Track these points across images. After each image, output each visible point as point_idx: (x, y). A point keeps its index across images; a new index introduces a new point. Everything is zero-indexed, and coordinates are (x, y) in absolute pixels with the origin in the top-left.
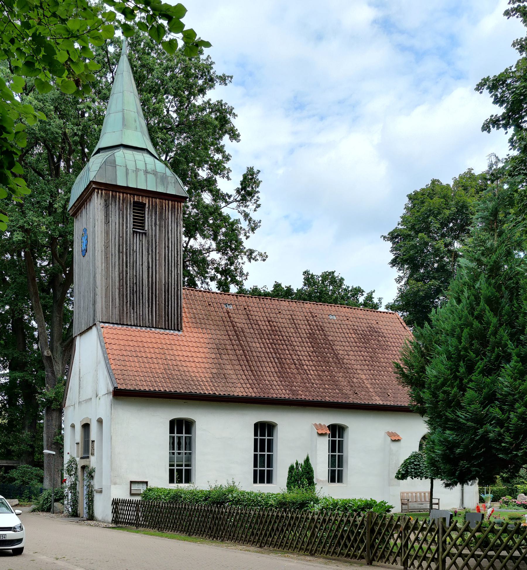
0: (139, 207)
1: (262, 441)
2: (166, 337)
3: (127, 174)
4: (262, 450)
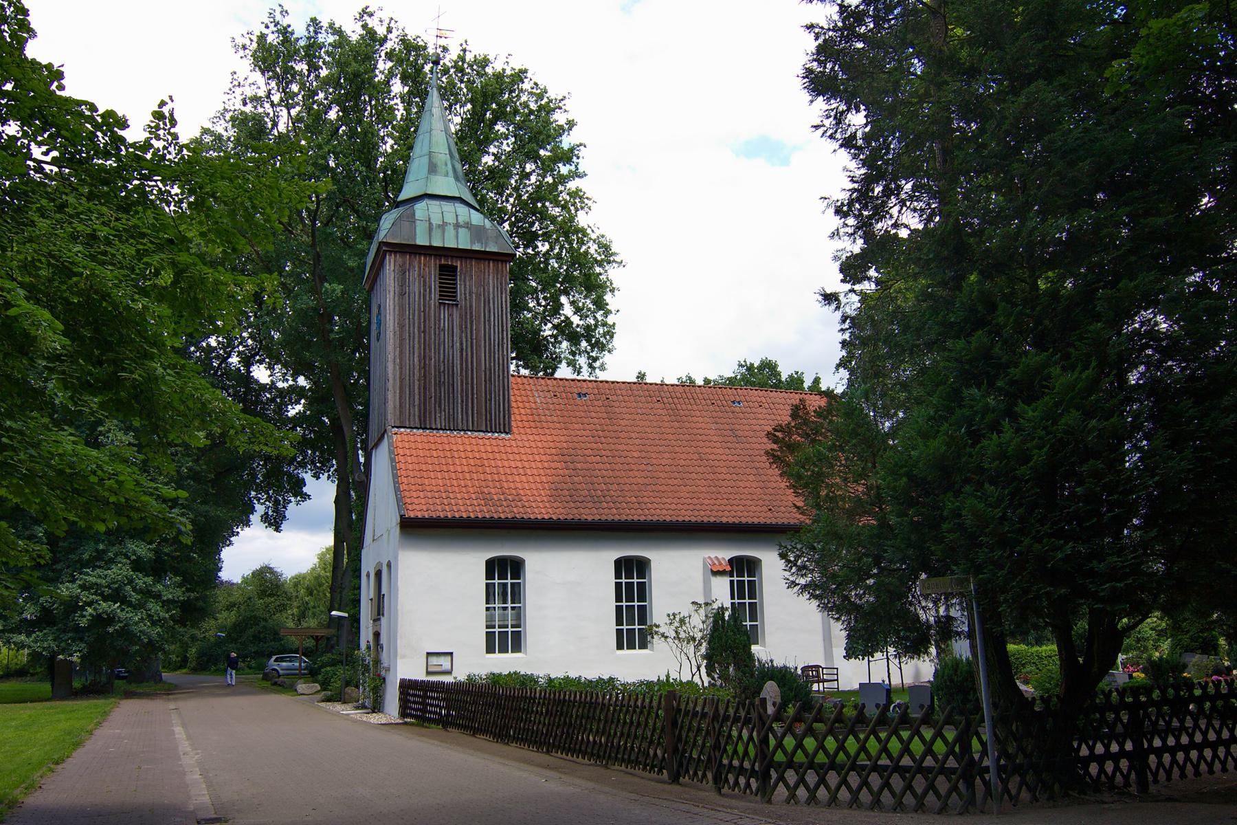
0: (447, 273)
1: (741, 583)
2: (487, 442)
3: (430, 229)
4: (741, 596)
